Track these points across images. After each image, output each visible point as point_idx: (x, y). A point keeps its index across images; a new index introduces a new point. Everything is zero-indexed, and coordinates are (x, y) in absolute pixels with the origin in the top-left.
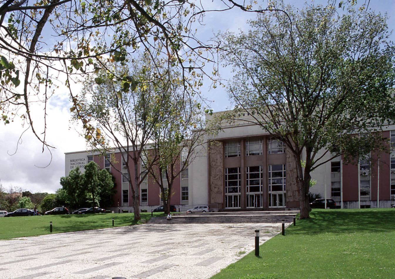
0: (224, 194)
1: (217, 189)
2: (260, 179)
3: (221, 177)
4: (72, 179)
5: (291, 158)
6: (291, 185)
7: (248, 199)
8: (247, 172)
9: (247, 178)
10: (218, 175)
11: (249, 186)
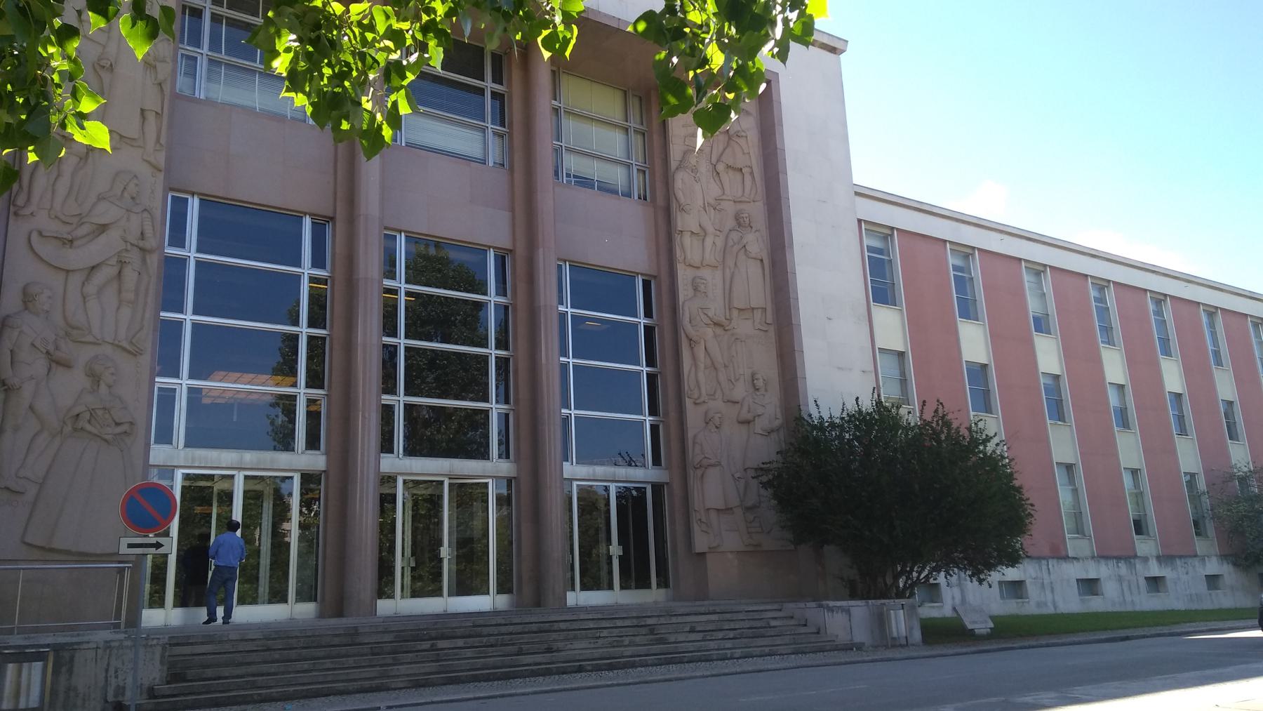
3: (134, 257)
10: (103, 228)
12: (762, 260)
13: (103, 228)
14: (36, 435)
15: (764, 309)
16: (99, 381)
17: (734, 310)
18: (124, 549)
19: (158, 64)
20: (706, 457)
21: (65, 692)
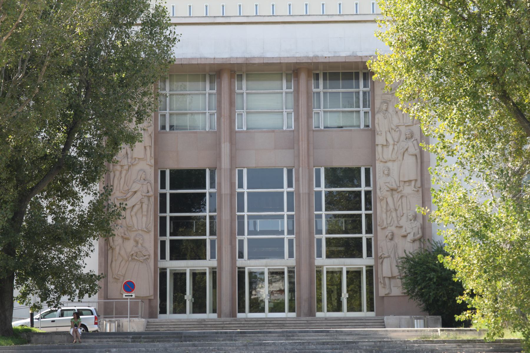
1: (132, 243)
2: (363, 212)
3: (145, 200)
4: (128, 142)
5: (391, 147)
6: (392, 239)
7: (319, 279)
8: (241, 186)
9: (241, 209)
10: (135, 192)
12: (416, 155)
13: (135, 192)
14: (121, 261)
18: (124, 297)
20: (383, 254)
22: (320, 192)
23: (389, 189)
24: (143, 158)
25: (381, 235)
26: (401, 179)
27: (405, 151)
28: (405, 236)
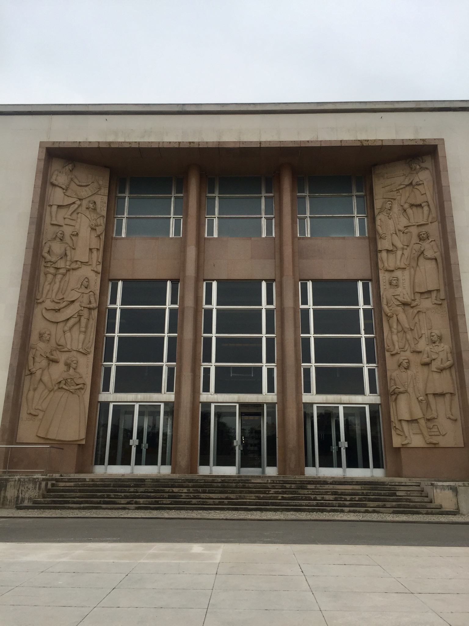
0: (94, 393)
1: (61, 367)
2: (312, 335)
3: (85, 313)
5: (399, 253)
11: (114, 364)
12: (436, 259)
15: (438, 291)
16: (70, 367)
17: (416, 294)
19: (97, 228)
21: (3, 498)
22: (307, 310)
23: (401, 304)
24: (87, 262)
25: (391, 363)
26: (417, 290)
27: (420, 255)
28: (427, 364)
